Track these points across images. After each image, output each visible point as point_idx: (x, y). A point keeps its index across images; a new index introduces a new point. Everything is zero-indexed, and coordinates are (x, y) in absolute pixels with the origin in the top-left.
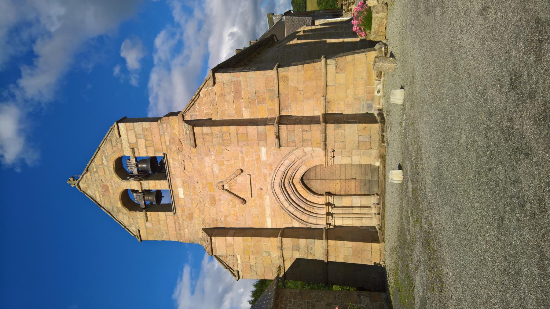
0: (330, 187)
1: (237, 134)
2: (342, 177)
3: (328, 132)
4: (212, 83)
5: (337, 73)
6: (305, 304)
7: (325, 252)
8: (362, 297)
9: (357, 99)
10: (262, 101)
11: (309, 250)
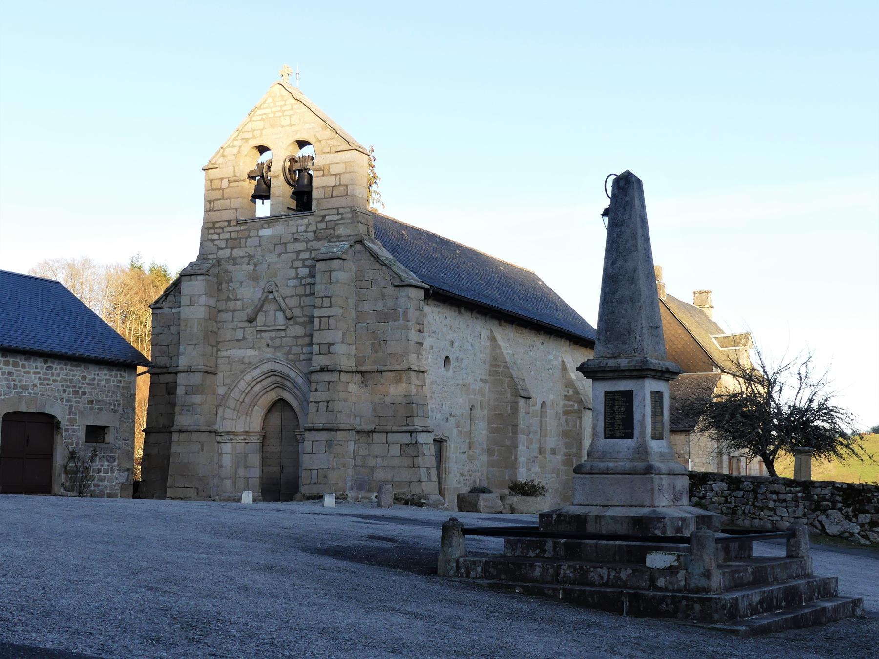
1: (329, 317)
4: (396, 283)
7: (184, 428)
8: (126, 473)
9: (372, 469)
11: (187, 408)
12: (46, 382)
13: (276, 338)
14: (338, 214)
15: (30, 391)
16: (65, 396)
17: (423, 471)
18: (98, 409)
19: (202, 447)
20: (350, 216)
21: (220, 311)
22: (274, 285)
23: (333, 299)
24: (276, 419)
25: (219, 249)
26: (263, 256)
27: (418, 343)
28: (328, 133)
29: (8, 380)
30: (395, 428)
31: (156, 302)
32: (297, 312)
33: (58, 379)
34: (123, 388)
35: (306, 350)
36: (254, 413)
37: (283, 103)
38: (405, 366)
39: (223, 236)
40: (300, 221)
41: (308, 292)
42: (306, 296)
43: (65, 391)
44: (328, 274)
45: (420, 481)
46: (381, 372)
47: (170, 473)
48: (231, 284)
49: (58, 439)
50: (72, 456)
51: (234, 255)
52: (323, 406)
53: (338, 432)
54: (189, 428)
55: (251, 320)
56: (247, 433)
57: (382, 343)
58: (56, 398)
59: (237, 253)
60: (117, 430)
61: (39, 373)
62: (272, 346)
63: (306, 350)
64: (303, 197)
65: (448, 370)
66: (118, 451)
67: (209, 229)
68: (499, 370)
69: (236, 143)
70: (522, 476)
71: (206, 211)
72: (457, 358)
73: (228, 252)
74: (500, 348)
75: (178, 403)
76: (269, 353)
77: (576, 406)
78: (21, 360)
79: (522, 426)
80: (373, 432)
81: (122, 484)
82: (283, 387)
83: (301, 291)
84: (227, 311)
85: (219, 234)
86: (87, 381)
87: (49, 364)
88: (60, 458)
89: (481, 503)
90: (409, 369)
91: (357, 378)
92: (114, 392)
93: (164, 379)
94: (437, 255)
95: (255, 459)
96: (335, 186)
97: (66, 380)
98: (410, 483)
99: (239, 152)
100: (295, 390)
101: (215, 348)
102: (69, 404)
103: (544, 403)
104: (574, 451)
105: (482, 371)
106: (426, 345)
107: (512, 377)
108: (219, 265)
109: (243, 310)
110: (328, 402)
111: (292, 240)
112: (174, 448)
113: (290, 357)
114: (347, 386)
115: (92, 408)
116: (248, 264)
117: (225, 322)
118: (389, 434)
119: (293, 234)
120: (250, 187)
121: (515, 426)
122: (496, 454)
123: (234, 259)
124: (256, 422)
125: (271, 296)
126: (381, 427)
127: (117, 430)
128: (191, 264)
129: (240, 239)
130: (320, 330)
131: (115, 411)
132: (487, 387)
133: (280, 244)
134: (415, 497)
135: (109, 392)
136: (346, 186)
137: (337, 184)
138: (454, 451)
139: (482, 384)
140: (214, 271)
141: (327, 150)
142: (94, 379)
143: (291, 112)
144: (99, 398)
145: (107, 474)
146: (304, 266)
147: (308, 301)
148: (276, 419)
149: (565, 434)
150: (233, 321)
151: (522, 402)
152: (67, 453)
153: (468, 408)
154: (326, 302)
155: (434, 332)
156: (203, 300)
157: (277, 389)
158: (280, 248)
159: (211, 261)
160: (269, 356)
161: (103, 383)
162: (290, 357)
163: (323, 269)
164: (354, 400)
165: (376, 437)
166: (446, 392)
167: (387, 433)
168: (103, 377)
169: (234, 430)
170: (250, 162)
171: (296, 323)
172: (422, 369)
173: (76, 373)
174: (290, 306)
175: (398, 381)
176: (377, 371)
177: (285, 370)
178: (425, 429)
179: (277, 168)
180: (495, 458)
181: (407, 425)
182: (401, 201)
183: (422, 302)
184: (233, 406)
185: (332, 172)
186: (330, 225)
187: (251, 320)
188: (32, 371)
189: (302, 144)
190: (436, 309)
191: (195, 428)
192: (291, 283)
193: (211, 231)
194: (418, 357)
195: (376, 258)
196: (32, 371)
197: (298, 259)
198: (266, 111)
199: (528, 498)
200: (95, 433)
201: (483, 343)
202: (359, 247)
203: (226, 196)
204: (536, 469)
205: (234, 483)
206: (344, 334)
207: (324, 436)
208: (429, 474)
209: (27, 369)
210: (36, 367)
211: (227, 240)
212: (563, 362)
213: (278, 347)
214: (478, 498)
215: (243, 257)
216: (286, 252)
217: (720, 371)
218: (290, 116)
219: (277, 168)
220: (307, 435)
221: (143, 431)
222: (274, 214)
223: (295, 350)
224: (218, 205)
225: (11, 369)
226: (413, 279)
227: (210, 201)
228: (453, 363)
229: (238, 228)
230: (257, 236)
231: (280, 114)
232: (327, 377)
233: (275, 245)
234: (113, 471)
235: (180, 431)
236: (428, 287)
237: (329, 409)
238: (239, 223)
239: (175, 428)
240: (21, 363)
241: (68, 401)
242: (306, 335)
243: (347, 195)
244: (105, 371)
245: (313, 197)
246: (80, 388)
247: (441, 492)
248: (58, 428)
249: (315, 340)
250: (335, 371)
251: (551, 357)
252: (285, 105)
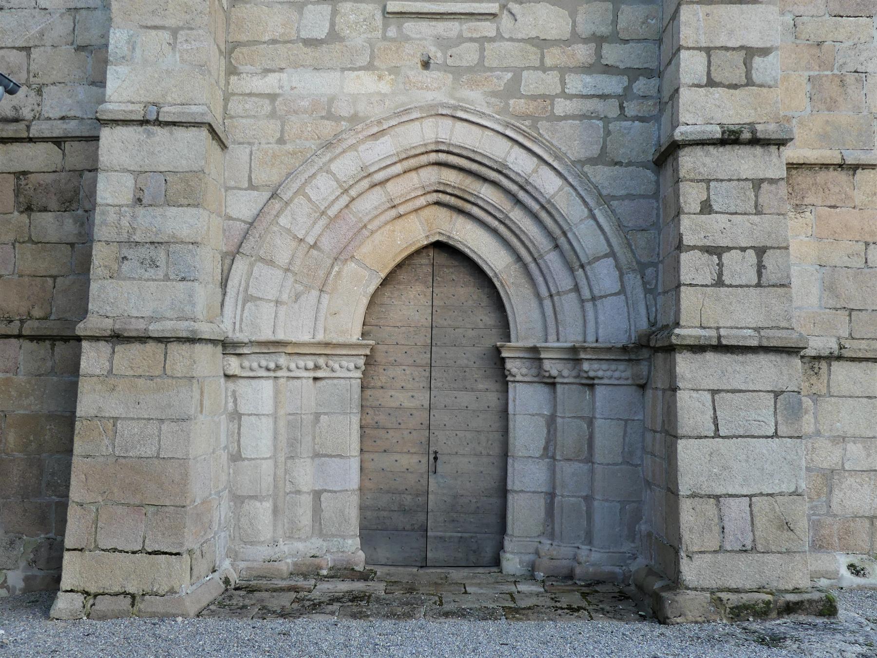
0: (395, 363)
2: (439, 417)
3: (763, 359)
7: (136, 327)
9: (829, 477)
10: (822, 96)
11: (143, 252)
13: (461, 39)
24: (412, 305)
46: (855, 168)
47: (76, 493)
52: (739, 267)
54: (155, 329)
57: (850, 79)
62: (445, 67)
82: (459, 206)
95: (347, 431)
110: (761, 251)
113: (517, 105)
124: (343, 315)
162: (517, 105)
169: (281, 336)
177: (496, 149)
184: (283, 258)
191: (183, 328)
213: (470, 69)
223: (532, 82)
235: (117, 338)
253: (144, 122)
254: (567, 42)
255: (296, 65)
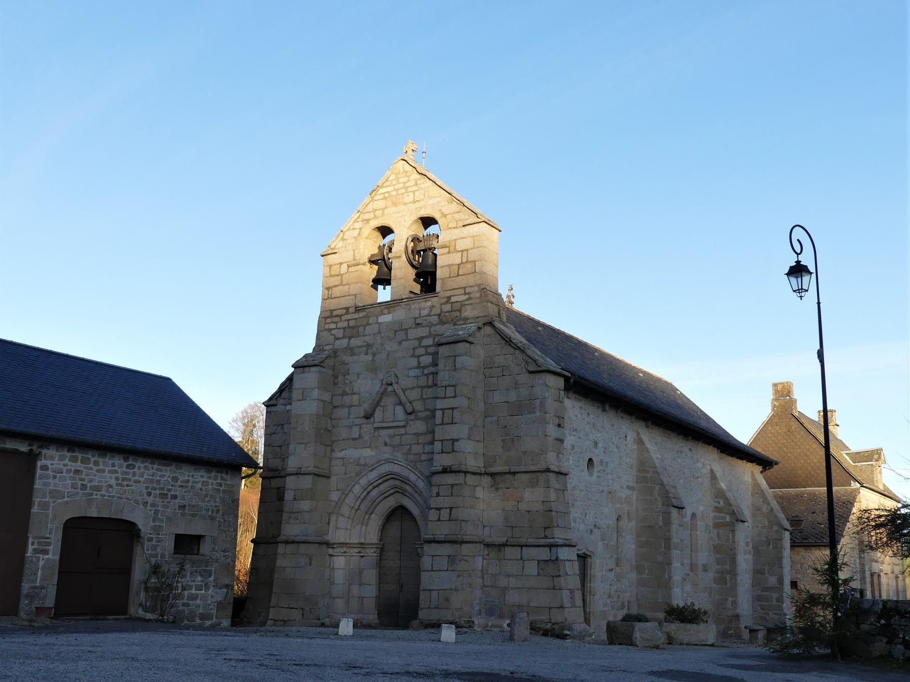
1: (453, 409)
3: (447, 545)
4: (531, 369)
5: (539, 561)
6: (216, 506)
8: (225, 590)
9: (505, 590)
12: (125, 483)
13: (395, 435)
14: (465, 294)
15: (103, 492)
16: (150, 500)
17: (566, 594)
18: (192, 515)
19: (311, 560)
20: (478, 295)
21: (335, 407)
22: (393, 376)
23: (458, 388)
24: (394, 530)
25: (337, 339)
26: (382, 345)
27: (557, 439)
28: (455, 206)
29: (74, 479)
30: (531, 541)
31: (271, 399)
32: (418, 406)
33: (142, 479)
34: (224, 491)
35: (428, 448)
36: (371, 521)
37: (406, 179)
38: (542, 466)
39: (340, 325)
40: (423, 305)
41: (430, 383)
42: (429, 387)
43: (149, 494)
44: (452, 359)
45: (562, 607)
46: (514, 473)
47: (274, 590)
48: (347, 377)
49: (138, 550)
50: (156, 570)
51: (352, 345)
52: (445, 514)
53: (464, 546)
54: (296, 539)
55: (368, 416)
56: (362, 545)
58: (137, 502)
59: (355, 342)
60: (214, 540)
61: (117, 472)
63: (428, 448)
64: (426, 277)
65: (591, 475)
66: (216, 565)
67: (326, 318)
68: (649, 477)
69: (357, 225)
70: (679, 599)
71: (324, 299)
72: (601, 461)
73: (345, 342)
74: (648, 451)
75: (286, 509)
76: (387, 453)
77: (728, 519)
78: (93, 456)
79: (675, 540)
80: (505, 545)
81: (219, 603)
82: (403, 493)
83: (423, 381)
84: (343, 406)
85: (336, 323)
86: (179, 483)
87: (130, 462)
88: (139, 571)
89: (637, 635)
90: (548, 470)
91: (486, 480)
92: (212, 497)
93: (275, 483)
94: (575, 354)
95: (371, 576)
96: (462, 263)
97: (152, 481)
98: (550, 608)
99: (359, 234)
100: (416, 495)
101: (329, 448)
102: (154, 509)
103: (694, 515)
104: (728, 567)
105: (629, 478)
106: (569, 441)
107: (662, 484)
108: (336, 357)
109: (360, 405)
110: (451, 509)
111: (414, 326)
112: (280, 562)
113: (411, 457)
114: (474, 490)
115: (183, 515)
116: (366, 354)
117: (340, 419)
118: (524, 549)
119: (415, 318)
120: (372, 272)
121: (668, 540)
122: (646, 572)
123: (352, 349)
124: (372, 533)
125: (390, 389)
126: (514, 540)
127: (214, 540)
128: (306, 356)
129: (359, 327)
130: (442, 424)
131: (212, 519)
132: (634, 495)
133: (401, 330)
134: (556, 627)
135: (206, 496)
136: (474, 262)
137: (464, 260)
138: (599, 568)
139: (629, 492)
140: (329, 362)
141: (453, 225)
142: (188, 481)
143: (415, 188)
144: (193, 503)
145: (201, 594)
146: (427, 354)
147: (430, 392)
148: (394, 530)
149: (717, 549)
150: (348, 418)
151: (674, 512)
152: (148, 566)
153: (615, 518)
154: (450, 392)
155: (575, 430)
156: (316, 393)
157: (396, 494)
158: (401, 335)
159: (326, 352)
160: (387, 456)
161: (199, 485)
162: (411, 457)
163: (447, 354)
164: (485, 507)
165: (509, 552)
166: (589, 499)
167: (522, 546)
168: (199, 478)
169: (348, 541)
170: (371, 246)
171: (418, 418)
172: (563, 471)
173: (166, 474)
174: (411, 398)
175: (534, 484)
176: (510, 473)
177: (405, 472)
178: (567, 543)
179: (399, 248)
180: (645, 576)
181: (546, 537)
182: (538, 297)
183: (562, 393)
184: (347, 514)
185: (459, 248)
186: (456, 307)
187: (368, 416)
188: (107, 469)
189: (428, 222)
190: (578, 404)
191: (303, 538)
192: (412, 373)
193: (329, 320)
194: (558, 456)
195: (508, 341)
196: (107, 469)
197: (420, 346)
198: (389, 189)
199: (689, 626)
200: (187, 544)
201: (629, 446)
202: (488, 330)
203: (344, 282)
204: (688, 588)
205: (347, 603)
206: (470, 429)
207: (446, 549)
208: (572, 598)
209: (101, 467)
210: (113, 465)
211: (344, 328)
212: (712, 471)
214: (633, 628)
215: (361, 347)
216: (407, 340)
217: (859, 485)
218: (414, 192)
219: (399, 248)
220: (426, 547)
221: (252, 541)
222: (395, 298)
224: (336, 292)
225: (79, 465)
226: (552, 365)
227: (328, 289)
228: (597, 466)
229: (356, 316)
230: (377, 323)
231: (403, 191)
232: (450, 479)
233: (396, 331)
234: (207, 587)
236: (569, 375)
237: (453, 517)
238: (358, 309)
239: (282, 538)
240: (92, 460)
241: (153, 505)
242: (428, 432)
243: (475, 272)
244: (202, 473)
245: (437, 277)
246: (169, 490)
247: (587, 621)
248: (139, 536)
249: (437, 437)
250: (459, 472)
251: (700, 465)
252: (409, 181)
253: (297, 474)
254: (425, 434)
255: (350, 447)
